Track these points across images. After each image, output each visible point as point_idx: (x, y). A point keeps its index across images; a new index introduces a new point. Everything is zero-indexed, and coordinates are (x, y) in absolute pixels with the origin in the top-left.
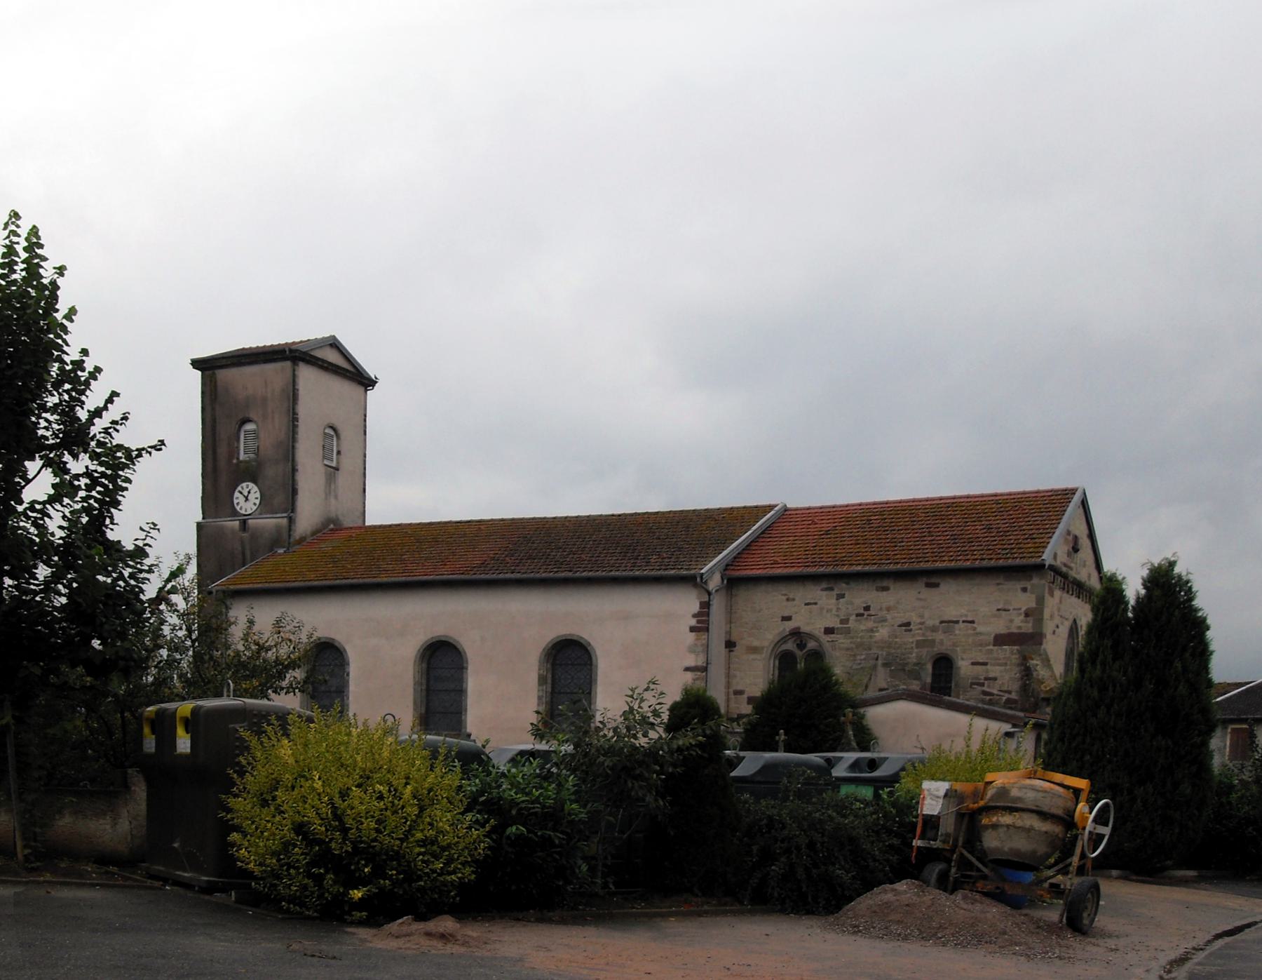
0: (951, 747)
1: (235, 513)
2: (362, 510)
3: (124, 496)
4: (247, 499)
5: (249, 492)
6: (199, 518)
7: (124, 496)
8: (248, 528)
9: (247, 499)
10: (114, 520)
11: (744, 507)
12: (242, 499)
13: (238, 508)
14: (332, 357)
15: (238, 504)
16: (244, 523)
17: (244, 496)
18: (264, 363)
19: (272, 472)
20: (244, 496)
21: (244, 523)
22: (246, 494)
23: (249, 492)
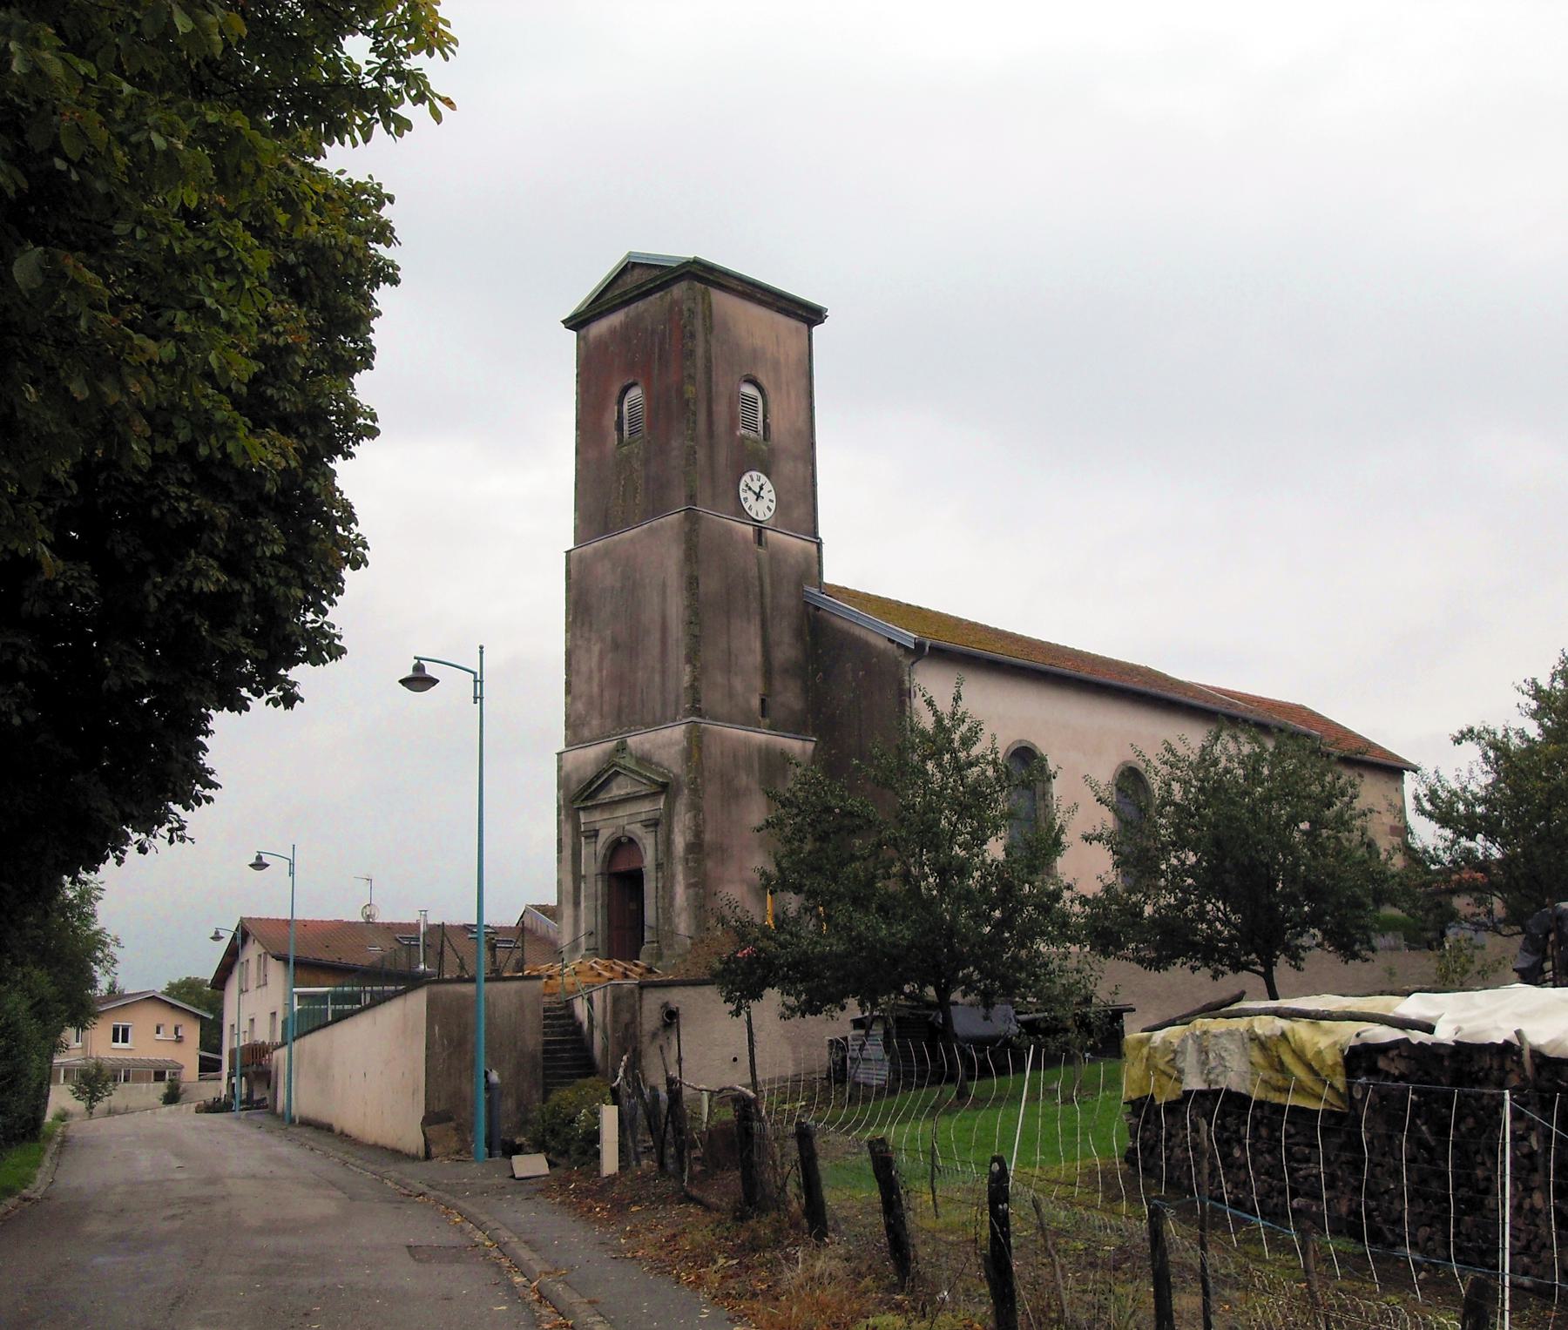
0: (935, 713)
1: (740, 512)
2: (801, 423)
3: (454, 53)
4: (758, 496)
5: (761, 488)
6: (562, 747)
7: (454, 53)
8: (766, 543)
9: (758, 496)
10: (363, 34)
11: (908, 605)
12: (752, 497)
13: (746, 507)
14: (1185, 1020)
15: (750, 508)
16: (759, 532)
17: (755, 493)
18: (777, 311)
19: (786, 467)
20: (755, 493)
21: (759, 532)
22: (757, 491)
23: (761, 488)
